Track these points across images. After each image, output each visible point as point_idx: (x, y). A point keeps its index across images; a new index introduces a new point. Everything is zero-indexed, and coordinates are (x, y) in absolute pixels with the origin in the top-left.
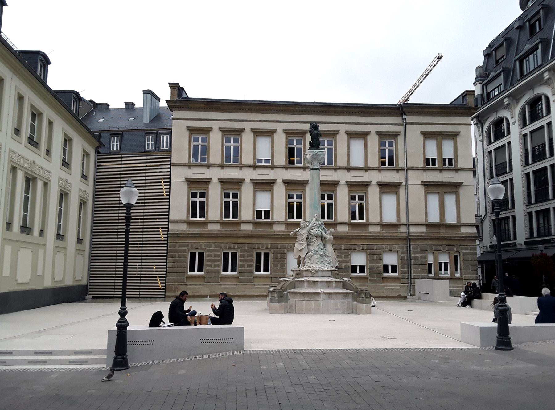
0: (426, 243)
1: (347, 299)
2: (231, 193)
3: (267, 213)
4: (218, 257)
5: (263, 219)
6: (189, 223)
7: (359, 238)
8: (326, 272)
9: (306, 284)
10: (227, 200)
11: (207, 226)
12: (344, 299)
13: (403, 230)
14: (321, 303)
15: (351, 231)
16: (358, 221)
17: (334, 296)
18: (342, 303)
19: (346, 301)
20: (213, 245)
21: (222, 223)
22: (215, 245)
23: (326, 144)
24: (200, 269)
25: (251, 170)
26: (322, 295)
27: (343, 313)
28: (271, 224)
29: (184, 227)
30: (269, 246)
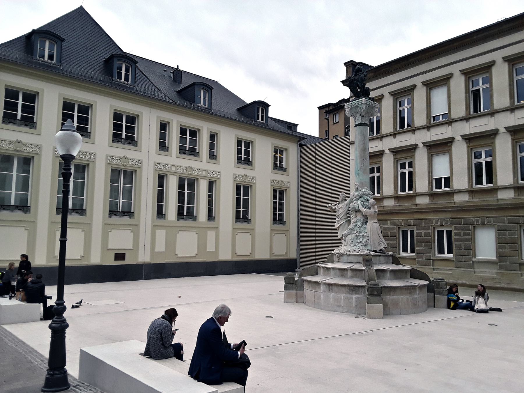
1: (356, 294)
2: (375, 168)
3: (448, 181)
5: (443, 189)
7: (488, 208)
8: (353, 257)
9: (388, 275)
10: (372, 175)
11: (383, 202)
12: (349, 293)
14: (321, 296)
15: (518, 197)
17: (335, 288)
18: (347, 298)
19: (354, 296)
20: (389, 222)
21: (397, 198)
22: (391, 222)
23: (406, 104)
24: (449, 252)
25: (424, 131)
26: (322, 285)
27: (348, 312)
28: (452, 194)
30: (449, 221)
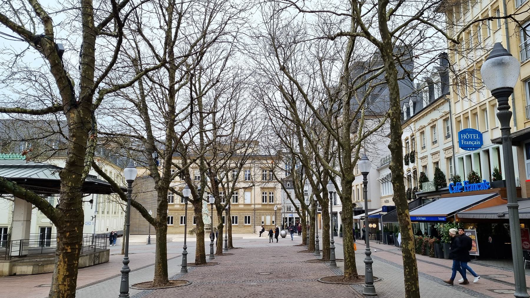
0: (261, 211)
4: (179, 218)
6: (263, 205)
13: (253, 206)
16: (265, 203)
29: (260, 206)
